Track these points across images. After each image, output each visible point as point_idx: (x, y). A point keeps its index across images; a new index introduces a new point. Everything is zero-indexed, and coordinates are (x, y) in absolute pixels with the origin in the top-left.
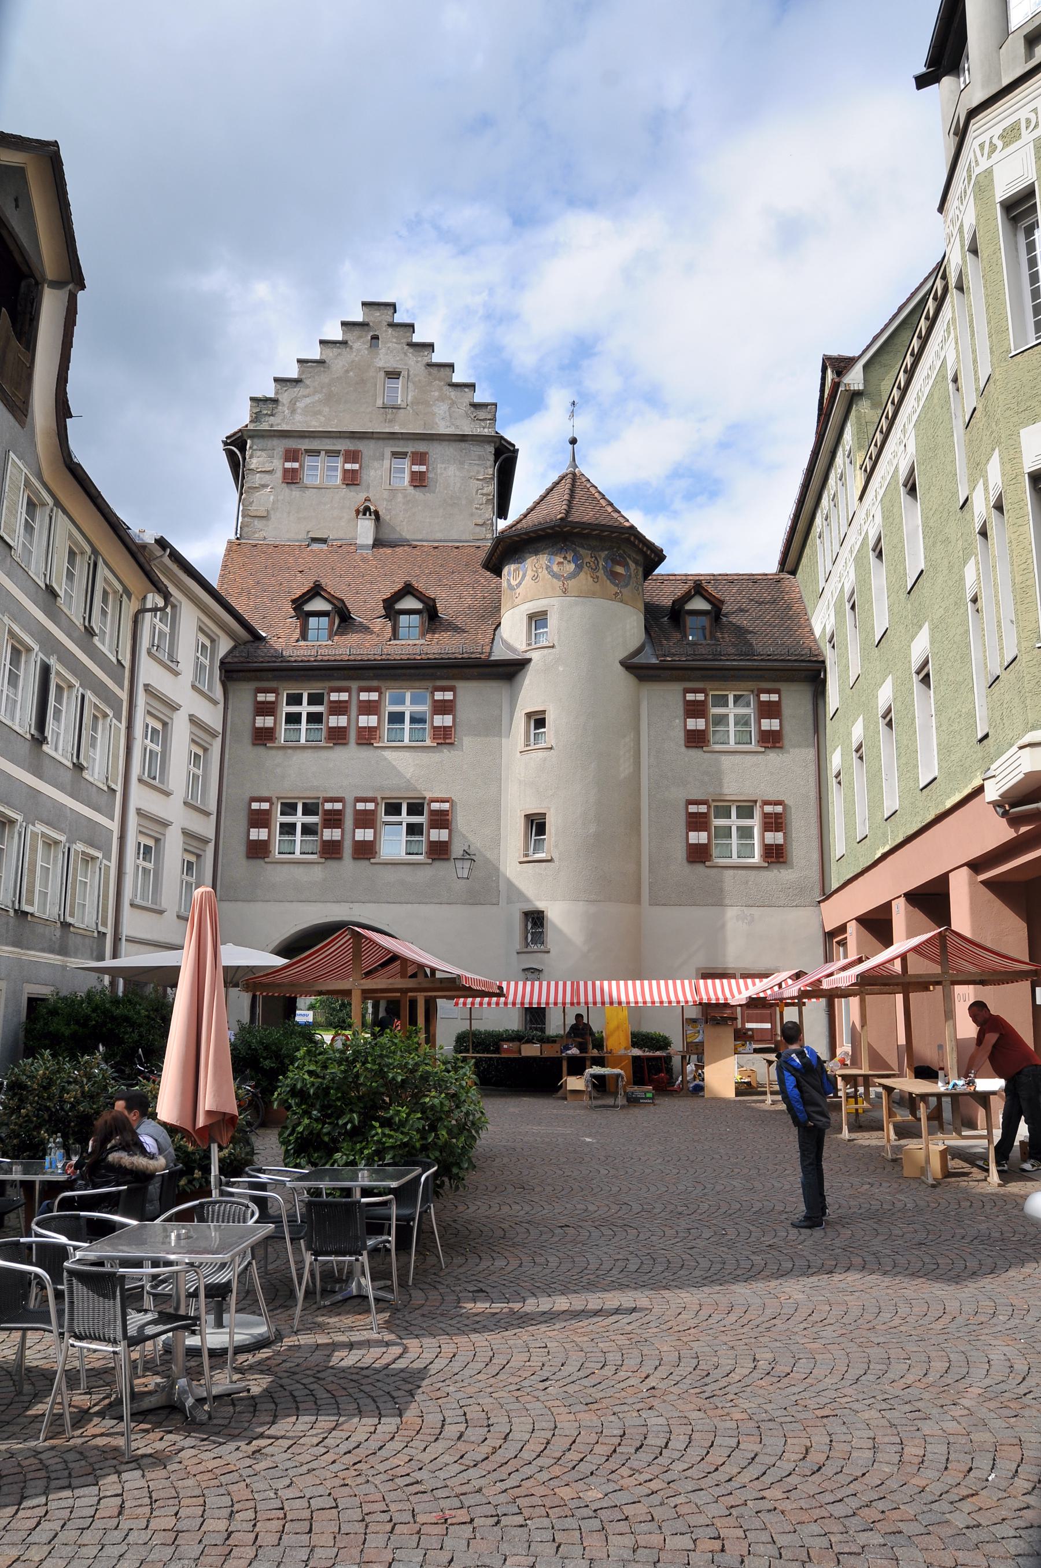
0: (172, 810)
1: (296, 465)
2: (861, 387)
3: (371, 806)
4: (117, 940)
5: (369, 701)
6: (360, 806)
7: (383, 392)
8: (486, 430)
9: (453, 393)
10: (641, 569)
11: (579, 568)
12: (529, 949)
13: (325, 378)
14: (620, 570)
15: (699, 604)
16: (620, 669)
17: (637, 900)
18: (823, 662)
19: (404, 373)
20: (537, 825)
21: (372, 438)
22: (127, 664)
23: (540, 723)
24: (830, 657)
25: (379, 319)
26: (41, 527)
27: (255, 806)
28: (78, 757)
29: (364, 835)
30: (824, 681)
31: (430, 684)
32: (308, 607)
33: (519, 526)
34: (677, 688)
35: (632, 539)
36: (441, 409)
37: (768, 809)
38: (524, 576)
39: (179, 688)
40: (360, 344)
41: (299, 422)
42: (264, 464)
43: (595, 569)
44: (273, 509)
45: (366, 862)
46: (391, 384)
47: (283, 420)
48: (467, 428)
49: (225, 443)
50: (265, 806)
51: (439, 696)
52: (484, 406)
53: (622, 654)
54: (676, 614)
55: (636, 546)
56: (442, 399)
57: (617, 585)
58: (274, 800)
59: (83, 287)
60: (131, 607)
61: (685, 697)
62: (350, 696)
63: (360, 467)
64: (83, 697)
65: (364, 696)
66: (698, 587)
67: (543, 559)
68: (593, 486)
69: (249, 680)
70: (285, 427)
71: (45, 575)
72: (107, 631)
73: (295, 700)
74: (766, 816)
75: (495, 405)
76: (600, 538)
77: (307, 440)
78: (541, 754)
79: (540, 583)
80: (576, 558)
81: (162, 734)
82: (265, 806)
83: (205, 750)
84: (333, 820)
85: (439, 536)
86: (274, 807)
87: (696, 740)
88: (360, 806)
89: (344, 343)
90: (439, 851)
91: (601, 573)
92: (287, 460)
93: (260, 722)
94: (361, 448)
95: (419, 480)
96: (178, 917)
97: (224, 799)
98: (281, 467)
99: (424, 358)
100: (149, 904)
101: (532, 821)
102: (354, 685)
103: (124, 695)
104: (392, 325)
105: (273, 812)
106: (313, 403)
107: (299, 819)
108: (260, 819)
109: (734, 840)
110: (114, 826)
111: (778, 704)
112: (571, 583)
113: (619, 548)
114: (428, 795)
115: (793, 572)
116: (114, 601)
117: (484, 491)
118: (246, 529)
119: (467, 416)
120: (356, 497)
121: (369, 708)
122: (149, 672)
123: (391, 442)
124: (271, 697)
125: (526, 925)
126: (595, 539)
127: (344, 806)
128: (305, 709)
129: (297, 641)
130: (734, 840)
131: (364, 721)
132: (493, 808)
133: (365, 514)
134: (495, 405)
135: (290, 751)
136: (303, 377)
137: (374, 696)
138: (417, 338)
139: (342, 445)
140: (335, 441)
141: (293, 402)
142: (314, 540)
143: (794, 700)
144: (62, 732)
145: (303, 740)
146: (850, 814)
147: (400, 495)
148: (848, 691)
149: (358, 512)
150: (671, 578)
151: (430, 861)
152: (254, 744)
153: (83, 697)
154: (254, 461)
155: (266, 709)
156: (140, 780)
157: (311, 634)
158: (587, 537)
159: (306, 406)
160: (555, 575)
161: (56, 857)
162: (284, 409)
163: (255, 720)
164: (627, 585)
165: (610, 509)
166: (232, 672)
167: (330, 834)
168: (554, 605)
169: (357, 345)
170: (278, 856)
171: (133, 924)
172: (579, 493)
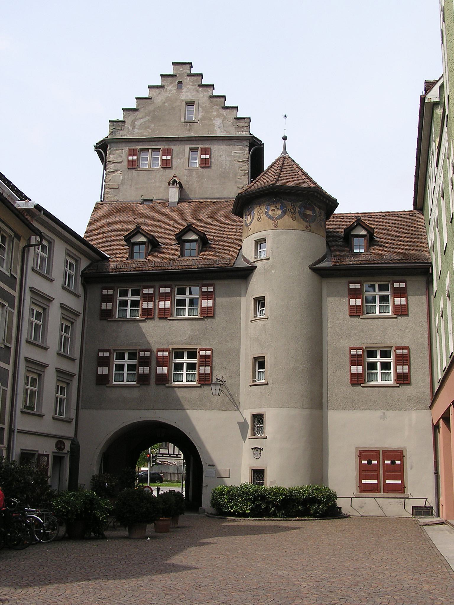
0: (51, 359)
1: (135, 158)
2: (438, 100)
3: (166, 354)
5: (165, 293)
8: (244, 133)
9: (225, 112)
10: (323, 212)
11: (284, 212)
12: (256, 437)
13: (151, 108)
14: (309, 212)
18: (431, 263)
19: (197, 102)
20: (260, 362)
22: (18, 277)
23: (262, 365)
27: (101, 354)
33: (250, 189)
34: (345, 280)
35: (316, 194)
37: (399, 351)
39: (54, 290)
40: (171, 88)
41: (137, 133)
42: (117, 158)
43: (294, 213)
44: (122, 183)
45: (163, 387)
46: (190, 109)
47: (127, 133)
48: (233, 132)
49: (96, 147)
50: (107, 354)
52: (244, 118)
54: (348, 237)
56: (218, 116)
57: (307, 222)
58: (112, 351)
61: (349, 286)
63: (172, 157)
65: (162, 290)
66: (359, 220)
67: (264, 209)
70: (129, 137)
72: (5, 258)
73: (124, 293)
74: (397, 356)
75: (250, 118)
78: (262, 322)
79: (262, 222)
80: (283, 206)
81: (42, 314)
82: (107, 354)
83: (72, 323)
84: (145, 362)
85: (217, 195)
86: (112, 355)
87: (355, 312)
89: (162, 87)
90: (205, 380)
91: (297, 215)
93: (104, 306)
94: (172, 147)
95: (205, 164)
97: (84, 351)
98: (126, 159)
99: (209, 92)
102: (157, 284)
103: (16, 294)
104: (190, 75)
105: (111, 358)
107: (126, 361)
108: (104, 362)
109: (379, 370)
110: (10, 367)
112: (279, 222)
116: (9, 241)
117: (243, 168)
118: (106, 196)
120: (169, 174)
121: (165, 297)
122: (33, 281)
124: (110, 292)
129: (127, 259)
130: (379, 370)
131: (162, 304)
132: (234, 354)
133: (173, 185)
134: (250, 118)
138: (204, 82)
142: (145, 200)
143: (415, 284)
145: (128, 317)
149: (169, 183)
150: (343, 216)
151: (398, 385)
152: (101, 319)
154: (111, 156)
155: (109, 299)
156: (27, 342)
160: (270, 217)
162: (128, 125)
164: (313, 222)
165: (304, 177)
168: (269, 234)
169: (170, 88)
170: (114, 383)
171: (22, 422)
172: (286, 169)
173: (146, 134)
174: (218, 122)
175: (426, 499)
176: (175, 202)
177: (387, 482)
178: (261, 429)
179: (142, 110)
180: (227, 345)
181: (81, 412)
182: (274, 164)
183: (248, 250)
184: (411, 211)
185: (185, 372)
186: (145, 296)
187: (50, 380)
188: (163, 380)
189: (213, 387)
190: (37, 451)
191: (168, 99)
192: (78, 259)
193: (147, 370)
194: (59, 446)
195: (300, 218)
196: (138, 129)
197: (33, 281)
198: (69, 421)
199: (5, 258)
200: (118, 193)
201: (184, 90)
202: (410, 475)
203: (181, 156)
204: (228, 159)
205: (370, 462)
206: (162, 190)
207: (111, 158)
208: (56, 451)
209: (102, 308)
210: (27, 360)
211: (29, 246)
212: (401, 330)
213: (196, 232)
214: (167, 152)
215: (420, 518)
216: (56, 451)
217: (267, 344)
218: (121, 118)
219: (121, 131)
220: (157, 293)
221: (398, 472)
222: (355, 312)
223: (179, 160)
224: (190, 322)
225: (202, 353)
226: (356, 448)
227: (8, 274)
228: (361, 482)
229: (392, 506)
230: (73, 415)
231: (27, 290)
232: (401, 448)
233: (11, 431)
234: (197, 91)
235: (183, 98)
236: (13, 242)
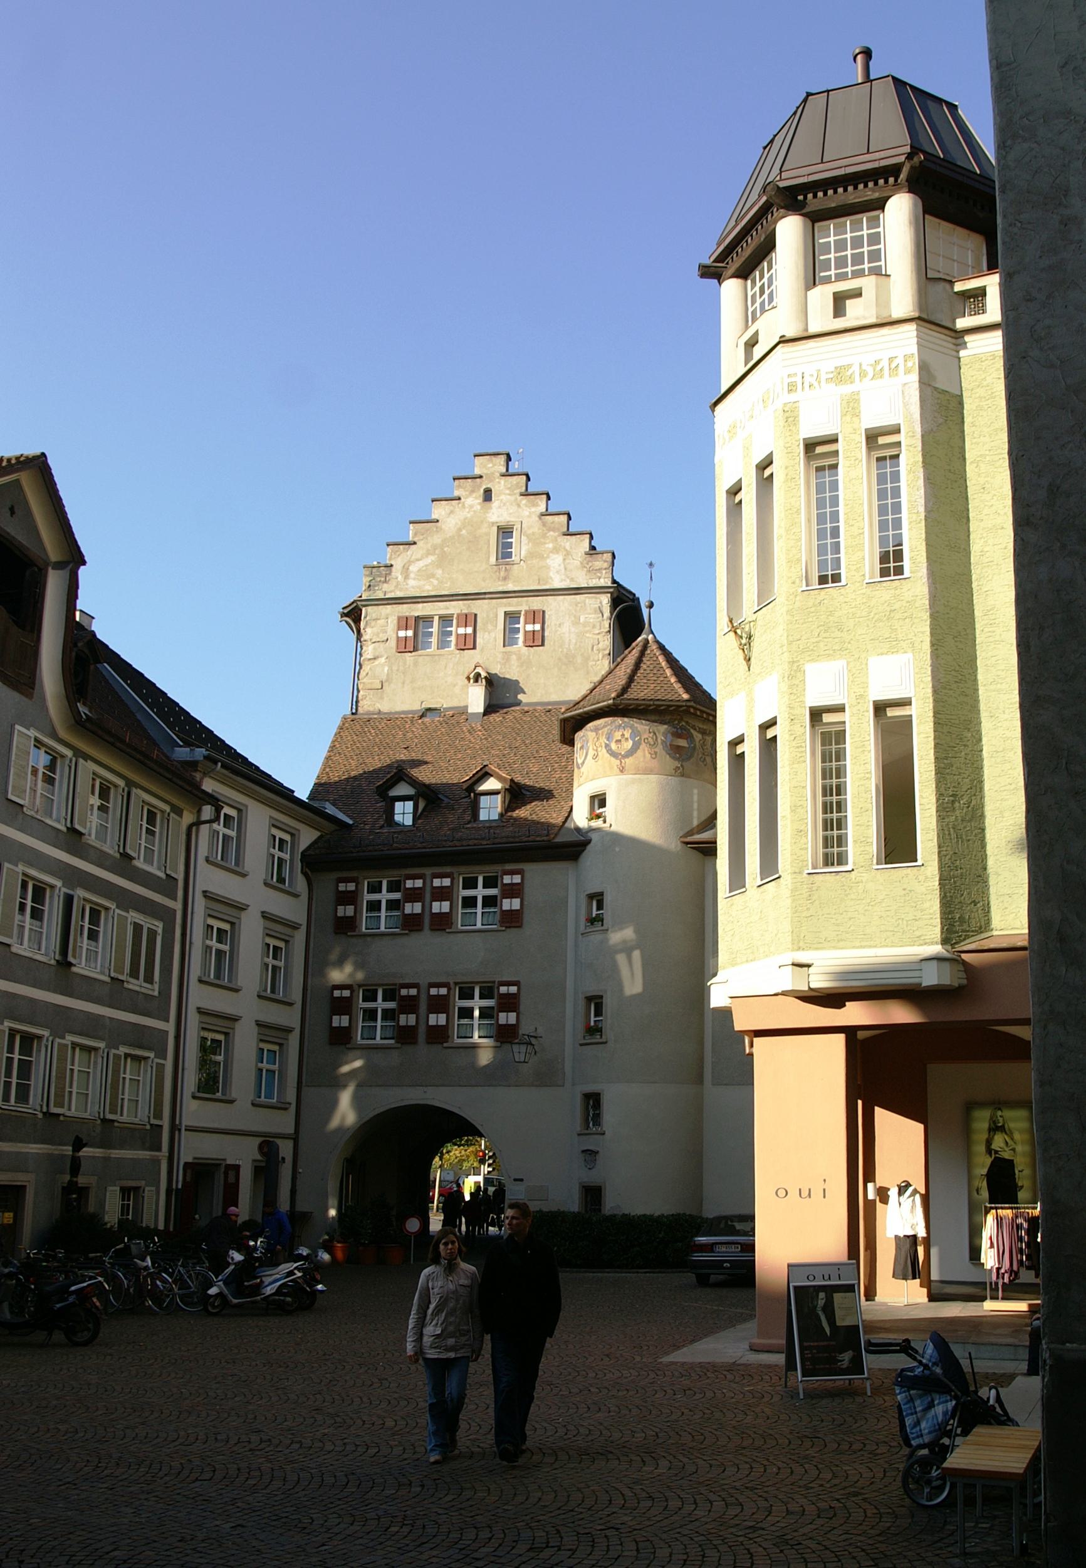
3: (443, 991)
6: (433, 991)
13: (437, 539)
14: (683, 743)
17: (699, 1079)
19: (517, 526)
22: (180, 877)
25: (492, 470)
26: (62, 776)
29: (437, 1019)
32: (393, 793)
36: (555, 561)
41: (413, 586)
42: (378, 635)
44: (387, 681)
47: (396, 586)
49: (343, 615)
56: (556, 550)
59: (84, 563)
60: (188, 818)
62: (424, 883)
65: (437, 882)
70: (399, 594)
72: (156, 849)
79: (600, 762)
84: (409, 1005)
86: (355, 994)
88: (433, 991)
96: (253, 1104)
102: (428, 871)
103: (178, 906)
110: (170, 1027)
113: (682, 719)
116: (162, 821)
121: (442, 894)
122: (208, 878)
124: (351, 887)
127: (418, 992)
128: (384, 896)
131: (436, 907)
135: (369, 939)
144: (100, 950)
149: (468, 678)
152: (336, 933)
155: (350, 898)
160: (613, 754)
161: (95, 1063)
163: (336, 909)
171: (193, 1111)
173: (428, 589)
178: (597, 1119)
179: (420, 544)
181: (304, 1089)
188: (439, 1035)
189: (516, 1048)
190: (225, 1160)
191: (466, 523)
193: (411, 1020)
194: (265, 1150)
197: (208, 878)
198: (282, 1107)
199: (156, 849)
200: (382, 698)
203: (490, 627)
204: (573, 629)
206: (457, 690)
207: (368, 633)
208: (259, 1157)
210: (200, 1011)
211: (198, 823)
216: (259, 1157)
220: (428, 889)
223: (486, 635)
227: (163, 876)
230: (291, 1096)
231: (199, 896)
233: (174, 1128)
234: (519, 506)
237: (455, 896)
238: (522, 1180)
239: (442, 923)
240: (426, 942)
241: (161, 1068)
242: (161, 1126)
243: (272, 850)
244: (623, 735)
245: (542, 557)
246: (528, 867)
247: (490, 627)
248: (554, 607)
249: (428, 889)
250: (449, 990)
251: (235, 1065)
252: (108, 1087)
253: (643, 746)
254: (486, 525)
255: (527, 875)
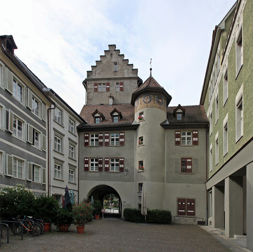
0: (65, 159)
1: (97, 87)
3: (108, 159)
4: (49, 186)
6: (106, 159)
7: (114, 68)
9: (128, 67)
10: (166, 101)
12: (140, 192)
14: (160, 101)
15: (180, 111)
16: (160, 125)
17: (164, 181)
18: (209, 122)
19: (118, 63)
20: (141, 163)
21: (112, 80)
23: (142, 140)
24: (210, 120)
27: (85, 159)
28: (27, 140)
29: (107, 166)
30: (209, 127)
31: (119, 132)
34: (173, 131)
38: (138, 103)
39: (65, 131)
40: (108, 56)
41: (97, 77)
43: (154, 100)
50: (87, 159)
51: (121, 134)
53: (161, 122)
55: (165, 94)
56: (126, 69)
57: (159, 105)
58: (89, 158)
60: (47, 107)
62: (103, 135)
64: (27, 125)
65: (106, 135)
67: (142, 99)
68: (157, 82)
69: (83, 131)
71: (4, 86)
76: (155, 92)
77: (98, 81)
78: (142, 147)
79: (142, 105)
82: (87, 159)
84: (101, 162)
85: (126, 102)
87: (178, 143)
88: (106, 159)
89: (105, 56)
92: (95, 86)
95: (122, 89)
96: (68, 182)
98: (94, 87)
100: (60, 179)
101: (141, 163)
102: (104, 132)
103: (46, 129)
104: (115, 50)
106: (99, 72)
108: (87, 162)
110: (46, 160)
111: (197, 134)
113: (160, 95)
114: (119, 157)
115: (203, 105)
119: (131, 72)
120: (108, 94)
121: (107, 137)
123: (116, 80)
124: (87, 135)
125: (139, 187)
126: (154, 92)
128: (95, 138)
135: (92, 147)
136: (97, 65)
137: (108, 135)
139: (106, 82)
140: (104, 81)
141: (95, 72)
142: (101, 104)
143: (201, 133)
145: (94, 145)
146: (214, 159)
147: (118, 93)
148: (215, 126)
149: (109, 97)
151: (120, 172)
153: (27, 125)
155: (87, 138)
157: (97, 122)
158: (152, 92)
159: (98, 73)
160: (145, 103)
161: (24, 165)
162: (94, 74)
164: (162, 105)
166: (80, 130)
167: (100, 166)
168: (144, 110)
169: (108, 56)
174: (126, 71)
175: (203, 219)
176: (111, 105)
177: (188, 211)
179: (98, 66)
180: (129, 156)
181: (80, 181)
182: (146, 80)
183: (137, 121)
184: (199, 105)
185: (94, 142)
186: (100, 137)
187: (66, 168)
188: (107, 169)
190: (62, 194)
192: (75, 121)
195: (157, 102)
196: (97, 75)
201: (113, 57)
202: (197, 209)
205: (182, 203)
207: (89, 87)
209: (85, 142)
211: (51, 109)
212: (196, 151)
213: (118, 112)
214: (108, 84)
215: (201, 225)
217: (144, 156)
218: (91, 70)
219: (91, 76)
220: (104, 136)
221: (193, 208)
222: (178, 143)
224: (116, 147)
225: (121, 159)
226: (177, 198)
228: (194, 211)
229: (190, 220)
230: (77, 183)
231: (52, 129)
232: (194, 198)
235: (113, 61)
236: (42, 105)
237: (110, 138)
238: (125, 202)
239: (107, 144)
240: (103, 148)
241: (44, 171)
242: (45, 185)
243: (70, 149)
244: (147, 98)
245: (123, 71)
246: (125, 132)
247: (113, 86)
248: (126, 82)
249: (104, 136)
250: (109, 159)
251: (64, 173)
252: (28, 172)
253: (152, 100)
254: (111, 62)
255: (125, 133)
